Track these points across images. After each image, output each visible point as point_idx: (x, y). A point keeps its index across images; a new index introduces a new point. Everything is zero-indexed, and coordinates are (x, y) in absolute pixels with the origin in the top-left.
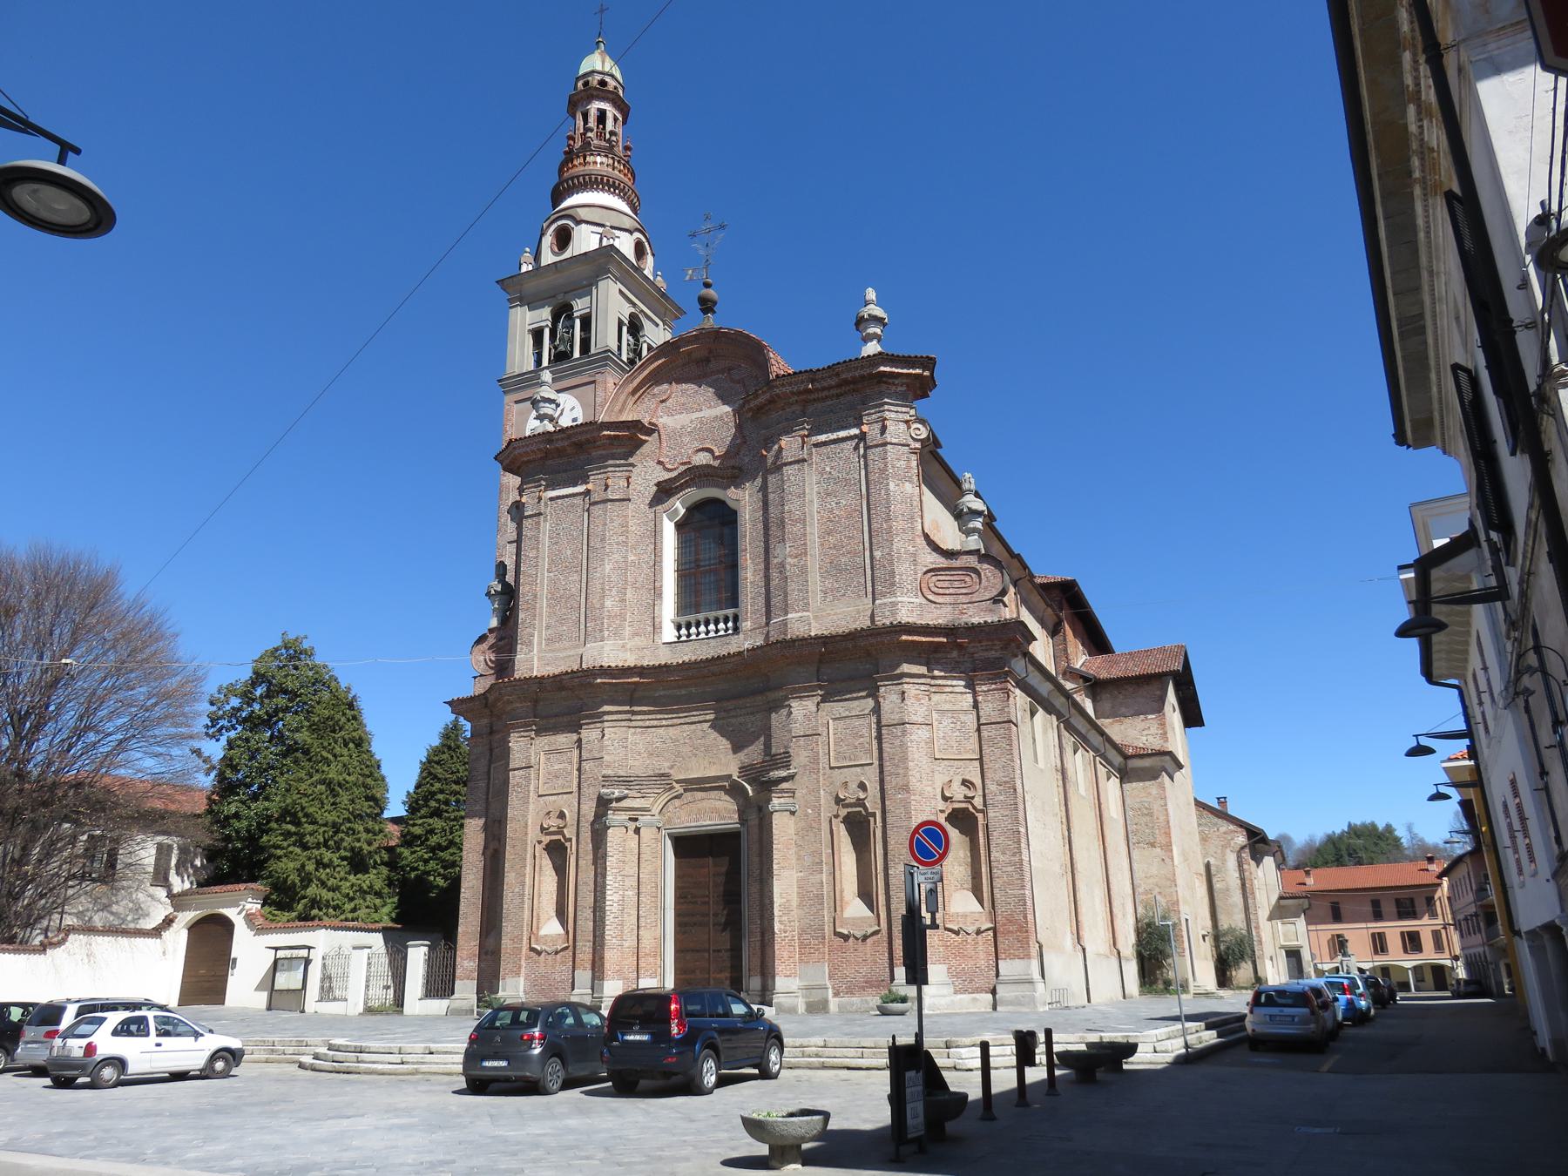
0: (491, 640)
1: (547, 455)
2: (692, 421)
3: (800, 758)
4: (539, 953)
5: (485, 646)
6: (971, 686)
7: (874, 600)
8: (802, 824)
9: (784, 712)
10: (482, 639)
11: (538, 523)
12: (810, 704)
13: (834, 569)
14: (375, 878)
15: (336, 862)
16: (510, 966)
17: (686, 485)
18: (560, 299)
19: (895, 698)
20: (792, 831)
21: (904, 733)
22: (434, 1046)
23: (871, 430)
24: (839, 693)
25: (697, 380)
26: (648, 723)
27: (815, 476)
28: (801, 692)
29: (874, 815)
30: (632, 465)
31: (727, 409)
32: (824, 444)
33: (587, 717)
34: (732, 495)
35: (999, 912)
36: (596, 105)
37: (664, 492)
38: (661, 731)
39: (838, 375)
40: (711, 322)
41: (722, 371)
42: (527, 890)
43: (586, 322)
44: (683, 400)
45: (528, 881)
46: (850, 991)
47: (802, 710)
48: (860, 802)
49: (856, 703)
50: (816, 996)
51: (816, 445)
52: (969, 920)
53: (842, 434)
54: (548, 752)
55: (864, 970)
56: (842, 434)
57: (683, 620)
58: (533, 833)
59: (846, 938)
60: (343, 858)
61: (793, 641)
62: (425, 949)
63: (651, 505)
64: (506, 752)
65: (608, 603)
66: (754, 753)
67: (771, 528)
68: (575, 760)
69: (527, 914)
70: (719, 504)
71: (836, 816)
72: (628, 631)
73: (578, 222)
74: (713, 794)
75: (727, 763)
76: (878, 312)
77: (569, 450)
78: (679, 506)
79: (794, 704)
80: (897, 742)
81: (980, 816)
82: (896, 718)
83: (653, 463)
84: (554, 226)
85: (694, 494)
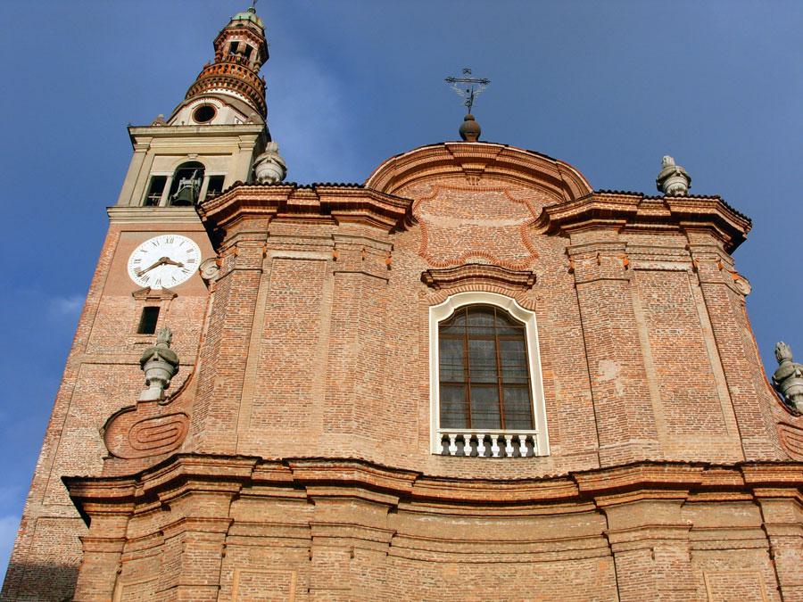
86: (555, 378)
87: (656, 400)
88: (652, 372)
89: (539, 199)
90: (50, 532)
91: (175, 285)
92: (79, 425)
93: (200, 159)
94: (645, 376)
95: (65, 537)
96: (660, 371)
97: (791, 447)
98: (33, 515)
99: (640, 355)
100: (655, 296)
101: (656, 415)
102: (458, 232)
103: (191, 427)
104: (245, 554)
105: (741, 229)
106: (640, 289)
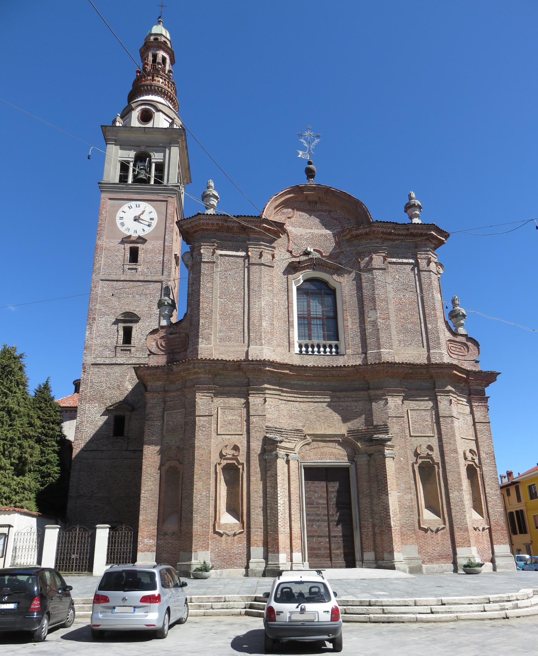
0: (162, 333)
1: (220, 229)
2: (307, 233)
3: (394, 429)
4: (221, 535)
5: (157, 336)
6: (469, 402)
7: (429, 350)
8: (398, 466)
9: (382, 402)
10: (154, 332)
11: (212, 268)
12: (398, 400)
13: (403, 330)
14: (28, 480)
15: (8, 466)
16: (200, 543)
17: (307, 267)
18: (143, 149)
19: (447, 403)
20: (394, 469)
21: (452, 422)
22: (445, 599)
23: (423, 263)
24: (413, 396)
25: (310, 211)
26: (289, 399)
27: (391, 280)
28: (394, 393)
29: (243, 464)
30: (274, 248)
31: (328, 232)
32: (394, 263)
33: (254, 389)
34: (334, 280)
35: (492, 520)
36: (161, 54)
37: (292, 268)
38: (296, 404)
39: (408, 229)
40: (313, 182)
41: (325, 211)
42: (212, 494)
43: (160, 168)
44: (301, 220)
45: (212, 489)
46: (431, 561)
47: (394, 402)
48: (235, 458)
49: (422, 403)
50: (415, 563)
51: (390, 263)
52: (479, 523)
53: (405, 261)
54: (224, 408)
55: (438, 549)
56: (405, 261)
57: (304, 342)
58: (215, 458)
59: (426, 530)
60: (12, 464)
61: (384, 363)
62: (58, 530)
63: (284, 273)
64: (193, 405)
65: (264, 324)
66: (358, 424)
67: (363, 303)
68: (245, 415)
69: (212, 509)
70: (324, 283)
71: (219, 464)
72: (275, 343)
73: (158, 110)
74: (331, 444)
75: (341, 429)
76: (418, 202)
77: (235, 230)
78: (300, 277)
79: (390, 399)
80: (449, 426)
81: (478, 469)
82: (447, 413)
83: (284, 250)
84: (143, 107)
85: (310, 273)
86: (349, 317)
87: (394, 332)
88: (393, 317)
89: (345, 218)
90: (98, 371)
91: (144, 234)
92: (105, 314)
93: (148, 150)
94: (389, 319)
95: (107, 373)
96: (396, 316)
97: (452, 352)
98: (88, 362)
99: (388, 308)
100: (397, 277)
101: (393, 338)
102: (305, 237)
103: (190, 342)
104: (222, 401)
105: (443, 239)
106: (391, 273)
